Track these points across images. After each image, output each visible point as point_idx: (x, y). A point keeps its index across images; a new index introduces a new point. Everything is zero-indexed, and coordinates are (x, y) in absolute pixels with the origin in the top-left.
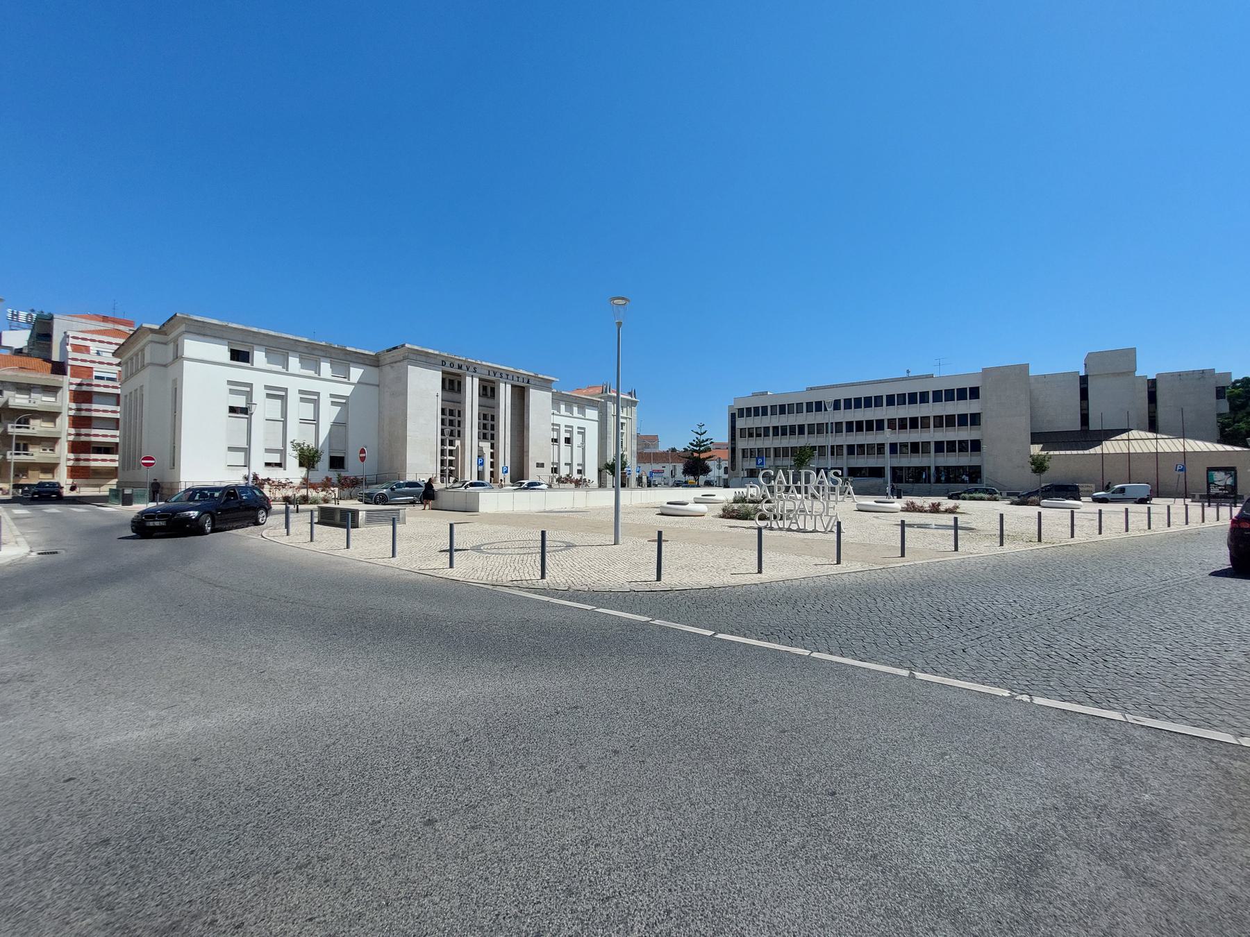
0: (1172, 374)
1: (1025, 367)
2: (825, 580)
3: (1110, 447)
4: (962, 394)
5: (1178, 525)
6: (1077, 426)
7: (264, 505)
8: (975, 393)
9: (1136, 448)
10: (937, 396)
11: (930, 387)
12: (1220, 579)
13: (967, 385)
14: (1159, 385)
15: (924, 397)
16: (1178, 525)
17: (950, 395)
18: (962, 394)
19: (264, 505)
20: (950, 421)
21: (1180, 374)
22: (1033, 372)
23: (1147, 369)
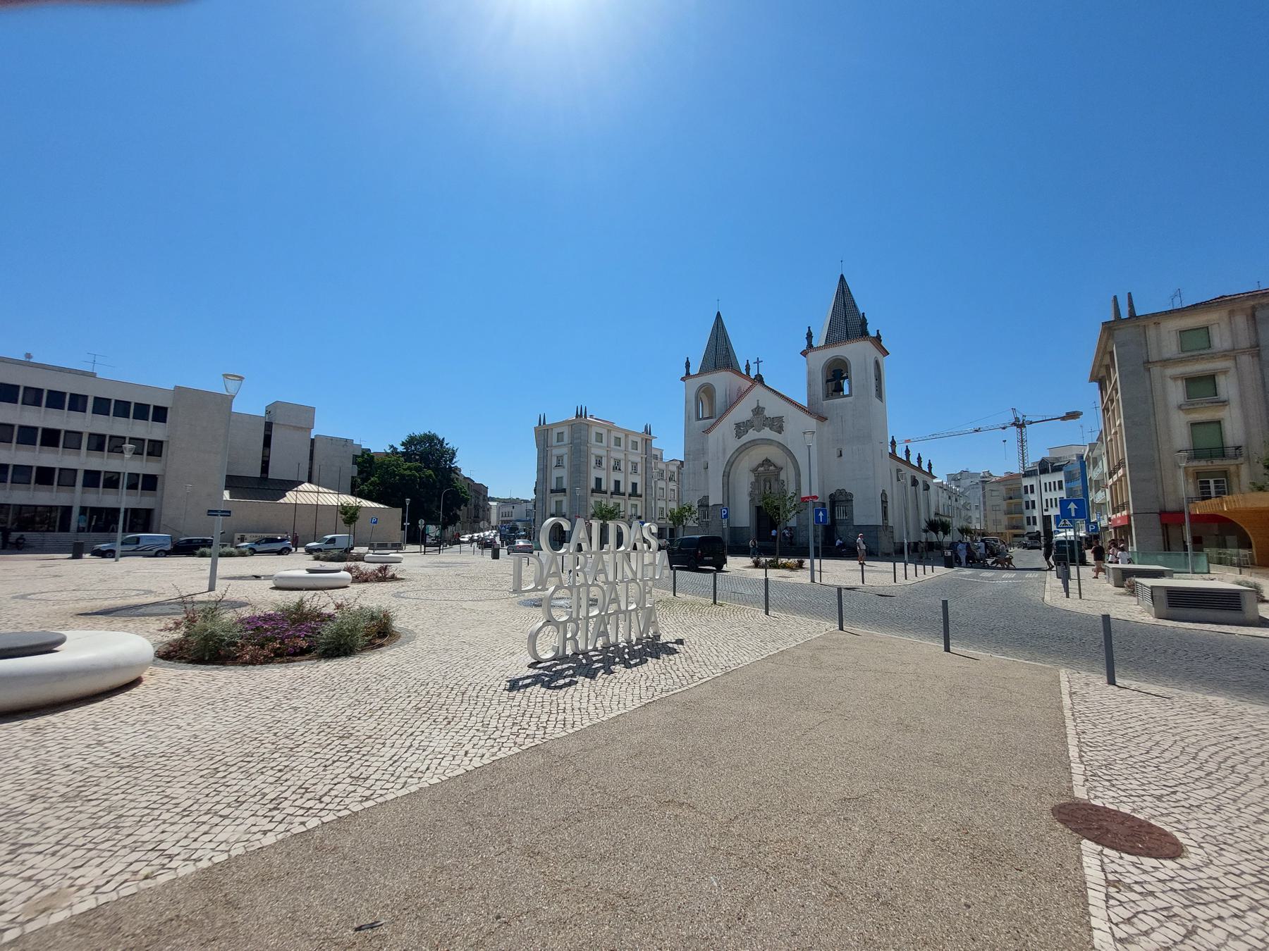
0: (326, 437)
1: (228, 400)
2: (131, 625)
3: (290, 497)
4: (141, 412)
5: (912, 579)
6: (257, 473)
7: (478, 517)
8: (160, 414)
9: (310, 499)
10: (102, 406)
11: (92, 391)
12: (244, 599)
13: (153, 401)
14: (317, 445)
15: (77, 403)
16: (912, 579)
17: (122, 409)
18: (141, 412)
19: (478, 517)
20: (51, 438)
21: (332, 439)
22: (237, 407)
23: (320, 429)
